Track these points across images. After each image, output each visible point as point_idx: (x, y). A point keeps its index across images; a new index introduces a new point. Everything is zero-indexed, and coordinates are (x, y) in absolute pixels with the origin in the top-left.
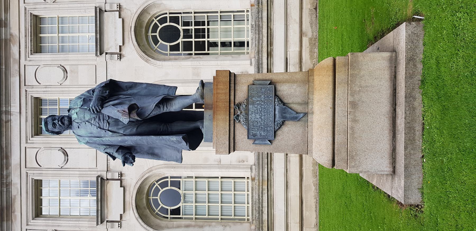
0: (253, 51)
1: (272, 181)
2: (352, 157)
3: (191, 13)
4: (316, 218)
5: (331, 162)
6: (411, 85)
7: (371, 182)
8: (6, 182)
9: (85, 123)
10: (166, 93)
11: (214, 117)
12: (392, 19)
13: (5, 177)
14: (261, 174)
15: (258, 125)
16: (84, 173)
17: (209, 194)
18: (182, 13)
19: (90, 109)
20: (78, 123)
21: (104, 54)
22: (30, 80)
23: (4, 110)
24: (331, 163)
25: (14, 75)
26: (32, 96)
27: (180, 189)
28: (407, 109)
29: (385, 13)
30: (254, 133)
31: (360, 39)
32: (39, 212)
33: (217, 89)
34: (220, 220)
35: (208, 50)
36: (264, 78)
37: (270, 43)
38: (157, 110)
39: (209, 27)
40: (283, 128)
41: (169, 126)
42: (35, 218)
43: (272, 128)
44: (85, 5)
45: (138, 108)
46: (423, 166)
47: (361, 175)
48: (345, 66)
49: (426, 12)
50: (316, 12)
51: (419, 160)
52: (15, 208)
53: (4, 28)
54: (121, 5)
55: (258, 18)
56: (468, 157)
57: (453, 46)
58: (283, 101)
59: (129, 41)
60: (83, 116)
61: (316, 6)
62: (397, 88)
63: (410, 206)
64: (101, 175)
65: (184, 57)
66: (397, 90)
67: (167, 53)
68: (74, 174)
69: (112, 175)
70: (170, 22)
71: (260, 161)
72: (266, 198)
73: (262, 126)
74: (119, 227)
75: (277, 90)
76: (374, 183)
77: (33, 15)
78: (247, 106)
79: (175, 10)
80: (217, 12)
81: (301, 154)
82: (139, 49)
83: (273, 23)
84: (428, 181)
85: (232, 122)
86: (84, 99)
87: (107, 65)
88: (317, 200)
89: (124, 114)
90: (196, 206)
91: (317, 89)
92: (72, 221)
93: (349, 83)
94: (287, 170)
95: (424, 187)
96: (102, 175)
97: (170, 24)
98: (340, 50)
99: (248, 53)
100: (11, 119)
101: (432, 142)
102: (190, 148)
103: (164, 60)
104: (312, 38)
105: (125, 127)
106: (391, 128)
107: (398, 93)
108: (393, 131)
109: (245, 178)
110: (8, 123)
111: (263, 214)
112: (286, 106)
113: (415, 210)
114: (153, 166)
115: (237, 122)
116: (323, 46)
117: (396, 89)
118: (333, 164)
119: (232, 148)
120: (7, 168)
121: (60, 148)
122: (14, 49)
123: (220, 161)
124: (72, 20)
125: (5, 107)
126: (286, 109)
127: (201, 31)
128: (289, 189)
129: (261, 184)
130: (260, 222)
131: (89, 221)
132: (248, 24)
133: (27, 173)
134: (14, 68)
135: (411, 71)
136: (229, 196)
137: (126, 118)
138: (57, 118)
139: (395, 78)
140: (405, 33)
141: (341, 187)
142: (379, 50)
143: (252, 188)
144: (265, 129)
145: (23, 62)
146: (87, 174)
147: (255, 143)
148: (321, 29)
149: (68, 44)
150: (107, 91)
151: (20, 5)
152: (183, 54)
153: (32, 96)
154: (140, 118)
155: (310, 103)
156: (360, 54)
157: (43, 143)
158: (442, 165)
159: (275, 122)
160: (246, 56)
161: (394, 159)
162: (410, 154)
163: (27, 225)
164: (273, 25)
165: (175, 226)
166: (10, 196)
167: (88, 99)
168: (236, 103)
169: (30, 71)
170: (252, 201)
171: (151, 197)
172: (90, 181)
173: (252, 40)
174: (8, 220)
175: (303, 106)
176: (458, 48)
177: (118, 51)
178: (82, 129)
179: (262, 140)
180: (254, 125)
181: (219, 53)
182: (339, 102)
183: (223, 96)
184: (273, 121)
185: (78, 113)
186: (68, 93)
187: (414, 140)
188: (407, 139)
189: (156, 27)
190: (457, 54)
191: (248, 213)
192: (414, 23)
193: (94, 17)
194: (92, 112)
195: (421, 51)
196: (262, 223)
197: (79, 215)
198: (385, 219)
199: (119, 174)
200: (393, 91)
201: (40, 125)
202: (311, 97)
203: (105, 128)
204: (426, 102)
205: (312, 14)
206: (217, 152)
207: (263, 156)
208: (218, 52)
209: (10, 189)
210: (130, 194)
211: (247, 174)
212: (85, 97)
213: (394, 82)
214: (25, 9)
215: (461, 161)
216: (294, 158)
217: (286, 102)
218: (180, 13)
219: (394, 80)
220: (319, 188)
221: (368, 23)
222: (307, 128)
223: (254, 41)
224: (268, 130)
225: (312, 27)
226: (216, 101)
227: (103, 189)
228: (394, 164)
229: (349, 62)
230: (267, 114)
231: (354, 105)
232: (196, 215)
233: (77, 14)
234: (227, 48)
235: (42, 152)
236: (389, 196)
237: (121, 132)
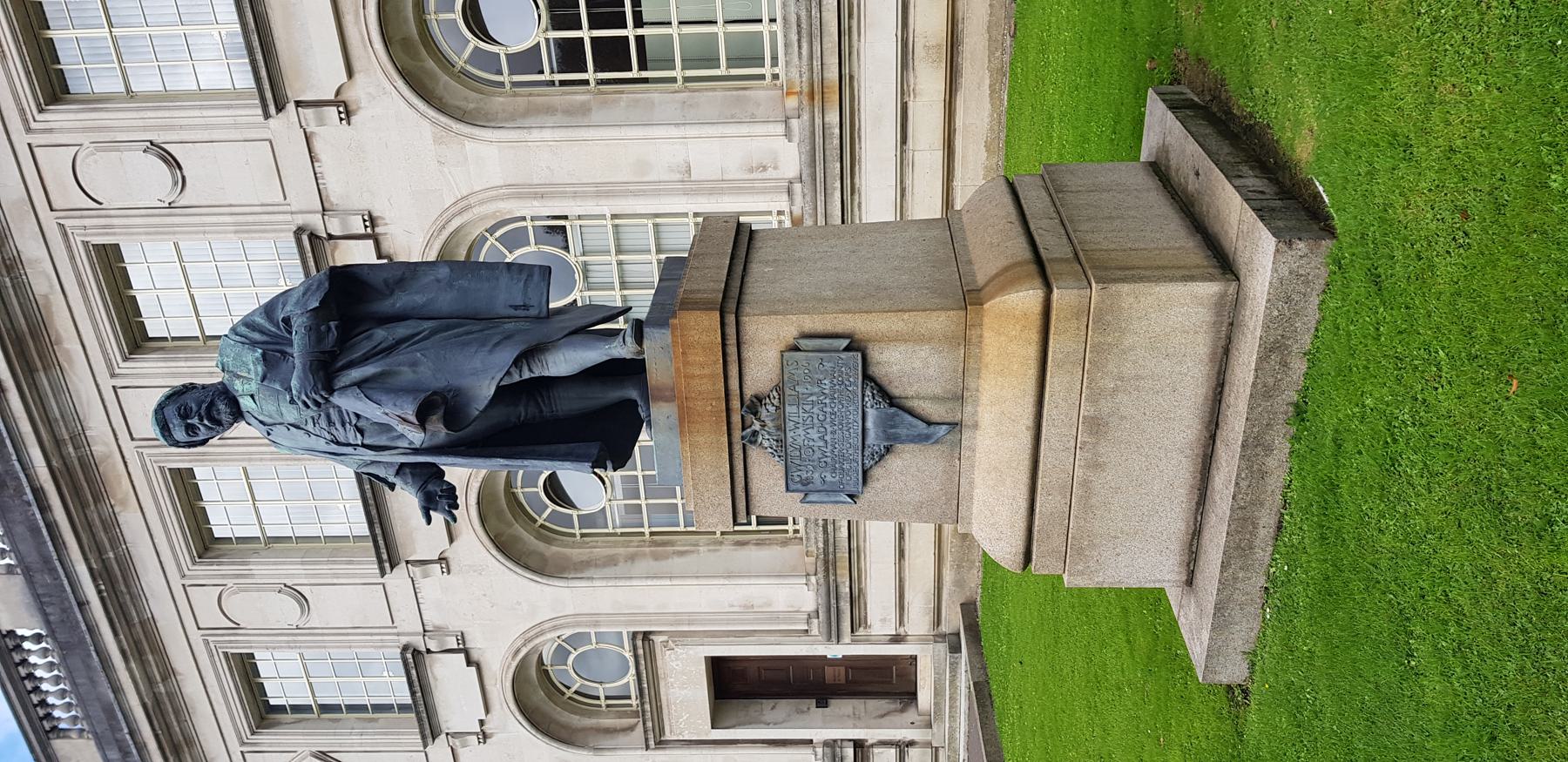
2: (1080, 551)
5: (1020, 558)
15: (815, 457)
27: (568, 252)
30: (804, 476)
32: (137, 335)
40: (890, 462)
41: (543, 401)
52: (57, 331)
64: (308, 225)
71: (818, 169)
73: (829, 460)
74: (344, 122)
75: (869, 360)
94: (903, 191)
106: (1197, 482)
110: (169, 680)
114: (470, 192)
118: (1027, 557)
121: (148, 144)
123: (689, 171)
133: (61, 226)
135: (1271, 381)
139: (1225, 354)
140: (1269, 273)
144: (837, 466)
146: (262, 224)
147: (808, 499)
155: (970, 400)
161: (1194, 555)
162: (1235, 579)
166: (32, 298)
174: (49, 365)
175: (950, 405)
184: (860, 448)
195: (1309, 325)
199: (365, 221)
201: (54, 64)
202: (972, 385)
203: (352, 442)
207: (827, 153)
209: (24, 277)
213: (1221, 366)
217: (897, 395)
219: (1222, 360)
222: (958, 462)
226: (686, 398)
228: (1192, 565)
229: (1092, 310)
230: (840, 429)
231: (1096, 426)
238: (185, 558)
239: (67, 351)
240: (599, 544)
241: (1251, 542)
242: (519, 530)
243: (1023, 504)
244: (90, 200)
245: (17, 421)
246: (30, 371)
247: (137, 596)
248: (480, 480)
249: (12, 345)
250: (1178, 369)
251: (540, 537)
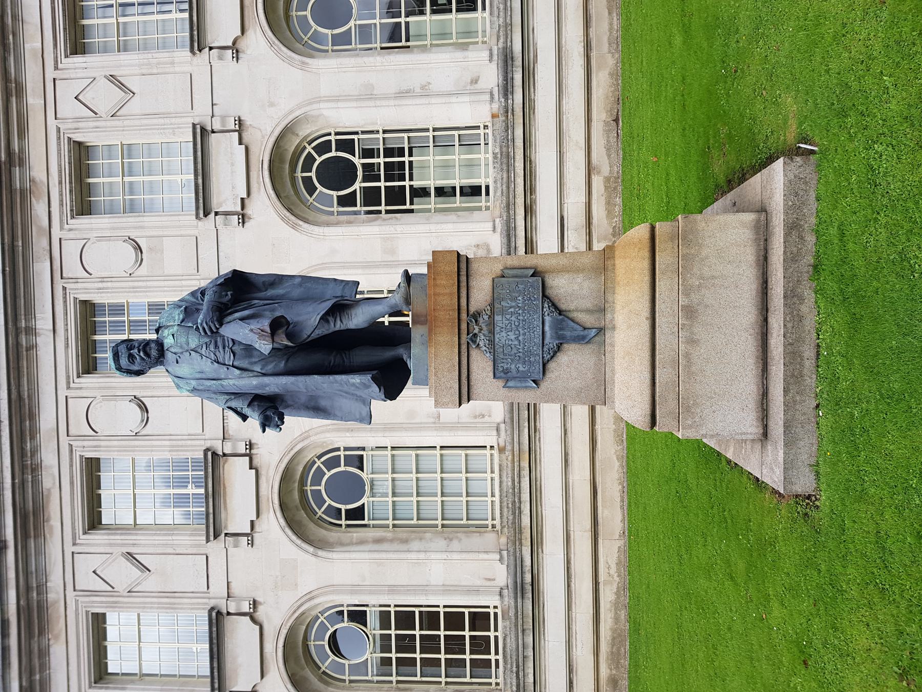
0: (498, 205)
1: (538, 453)
2: (688, 409)
3: (378, 132)
4: (623, 521)
5: (648, 419)
6: (796, 274)
7: (724, 454)
8: (31, 463)
9: (190, 354)
10: (339, 294)
11: (430, 339)
12: (758, 149)
13: (29, 455)
14: (516, 439)
15: (513, 352)
16: (180, 443)
17: (418, 479)
18: (360, 132)
19: (197, 327)
20: (175, 353)
21: (213, 214)
22: (72, 267)
23: (23, 325)
24: (650, 421)
25: (39, 258)
26: (75, 299)
27: (363, 471)
28: (788, 319)
29: (747, 137)
30: (505, 367)
31: (700, 183)
33: (435, 285)
34: (440, 527)
35: (412, 203)
36: (522, 264)
37: (530, 188)
38: (324, 327)
39: (411, 159)
41: (346, 357)
42: (88, 530)
43: (538, 358)
44: (173, 120)
45: (288, 323)
46: (818, 424)
47: (705, 440)
48: (672, 239)
49: (821, 139)
50: (618, 127)
51: (811, 412)
52: (49, 513)
53: (18, 168)
54: (242, 118)
55: (505, 141)
56: (896, 409)
57: (869, 206)
58: (558, 306)
59: (259, 189)
60: (185, 340)
61: (617, 114)
62: (769, 280)
63: (796, 498)
65: (365, 219)
66: (769, 284)
67: (333, 212)
68: (143, 446)
69: (234, 447)
70: (336, 150)
72: (526, 484)
73: (521, 354)
74: (250, 545)
76: (730, 455)
77: (74, 141)
78: (492, 316)
79: (346, 127)
80: (427, 130)
81: (593, 404)
82: (280, 205)
83: (535, 149)
84: (828, 451)
85: (464, 347)
86: (186, 308)
87: (219, 236)
88: (624, 487)
89: (263, 335)
90: (394, 502)
91: (620, 283)
92: (159, 535)
93: (681, 270)
95: (820, 462)
96: (215, 446)
97: (338, 155)
98: (663, 202)
99: (487, 208)
100: (38, 343)
101: (834, 380)
102: (385, 397)
103: (328, 224)
104: (611, 177)
105: (264, 359)
107: (772, 289)
108: (762, 360)
109: (486, 447)
110: (32, 351)
111: (522, 516)
112: (564, 315)
113: (804, 504)
114: (310, 428)
115: (474, 347)
116: (632, 195)
117: (767, 281)
119: (465, 397)
120: (33, 438)
122: (39, 209)
123: (439, 417)
124: (149, 149)
125: (26, 321)
126: (564, 321)
127: (396, 167)
128: (570, 468)
129: (516, 459)
130: (517, 530)
131: (191, 535)
132: (486, 152)
133: (71, 446)
134: (39, 244)
135: (795, 249)
136: (457, 481)
137: (266, 342)
138: (137, 345)
141: (668, 462)
142: (736, 208)
143: (500, 466)
144: (526, 359)
145: (56, 233)
146: (186, 446)
147: (508, 385)
148: (627, 159)
149: (142, 197)
150: (229, 293)
151: (48, 123)
152: (362, 212)
153: (75, 299)
154: (292, 343)
155: (609, 310)
156: (699, 217)
157: (100, 388)
158: (851, 422)
159: (543, 346)
160: (485, 214)
162: (795, 402)
163: (74, 544)
164: (535, 152)
165: (354, 541)
166: (41, 491)
167: (194, 308)
168: (471, 313)
169: (71, 251)
170: (501, 491)
171: (308, 486)
172: (192, 459)
173: (495, 182)
175: (596, 315)
176: (877, 209)
177: (239, 209)
178: (184, 365)
179: (520, 380)
180: (505, 352)
181: (433, 208)
182: (663, 306)
183: (448, 301)
184: (541, 345)
185: (175, 335)
186: (144, 292)
187: (802, 376)
188: (789, 374)
189: (310, 159)
190: (876, 220)
191: (492, 514)
192: (798, 159)
193: (192, 143)
194: (203, 334)
196: (521, 532)
197: (172, 523)
198: (750, 521)
199: (246, 445)
200: (763, 285)
201: (93, 353)
202: (610, 299)
203: (227, 363)
204: (822, 305)
205: (609, 130)
206: (437, 404)
208: (430, 206)
210: (267, 481)
211: (490, 439)
212: (188, 305)
213: (764, 269)
214: (58, 130)
215: (885, 416)
216: (580, 413)
217: (564, 309)
218: (356, 133)
219: (763, 265)
220: (628, 464)
221: (715, 153)
222: (603, 357)
223: (499, 185)
224: (530, 362)
225: (609, 156)
227: (216, 473)
228: (765, 420)
230: (529, 332)
231: (690, 312)
232: (394, 519)
233: (156, 138)
234: (448, 198)
235: (99, 405)
236: (757, 479)
237: (258, 368)
238: (85, 682)
239: (51, 528)
240: (361, 688)
241: (801, 371)
242: (308, 673)
243: (647, 375)
244: (91, 430)
245: (8, 570)
246: (26, 536)
247: (30, 312)
248: (288, 628)
249: (20, 518)
250: (737, 271)
251: (321, 680)
